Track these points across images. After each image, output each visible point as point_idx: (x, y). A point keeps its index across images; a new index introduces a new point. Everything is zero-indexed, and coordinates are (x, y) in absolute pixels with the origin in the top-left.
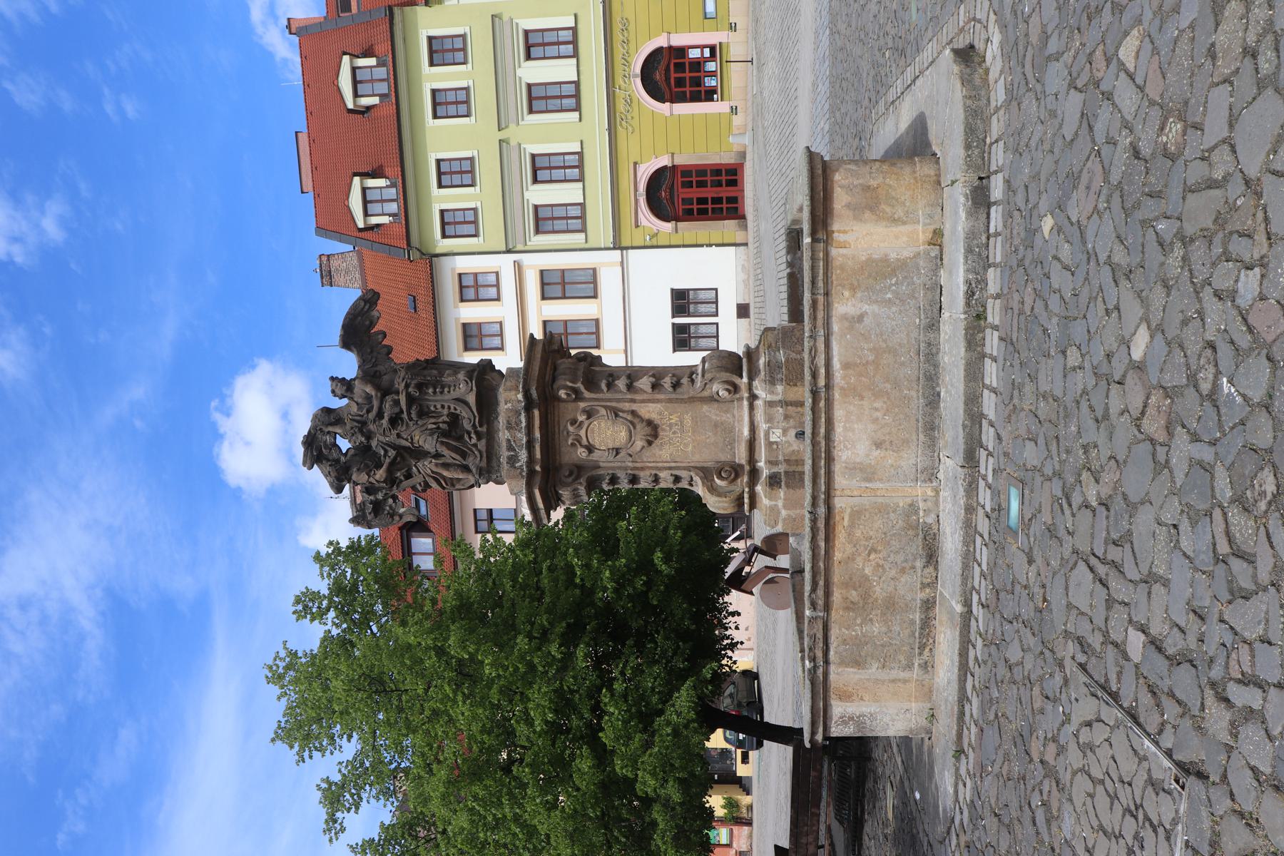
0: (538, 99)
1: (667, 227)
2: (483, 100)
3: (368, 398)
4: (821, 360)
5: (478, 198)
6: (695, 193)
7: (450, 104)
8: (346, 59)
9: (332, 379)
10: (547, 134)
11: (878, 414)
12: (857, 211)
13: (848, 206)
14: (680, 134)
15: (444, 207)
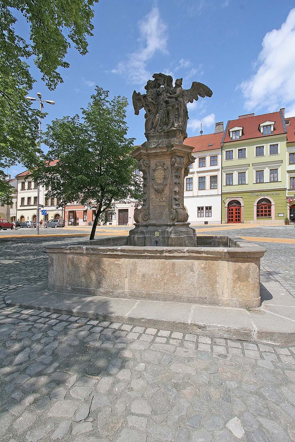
0: (260, 174)
1: (226, 205)
2: (260, 159)
3: (175, 93)
4: (176, 254)
5: (236, 160)
6: (234, 212)
7: (260, 152)
8: (274, 123)
9: (182, 79)
10: (251, 176)
11: (155, 277)
12: (237, 271)
13: (240, 268)
14: (249, 208)
15: (234, 151)
